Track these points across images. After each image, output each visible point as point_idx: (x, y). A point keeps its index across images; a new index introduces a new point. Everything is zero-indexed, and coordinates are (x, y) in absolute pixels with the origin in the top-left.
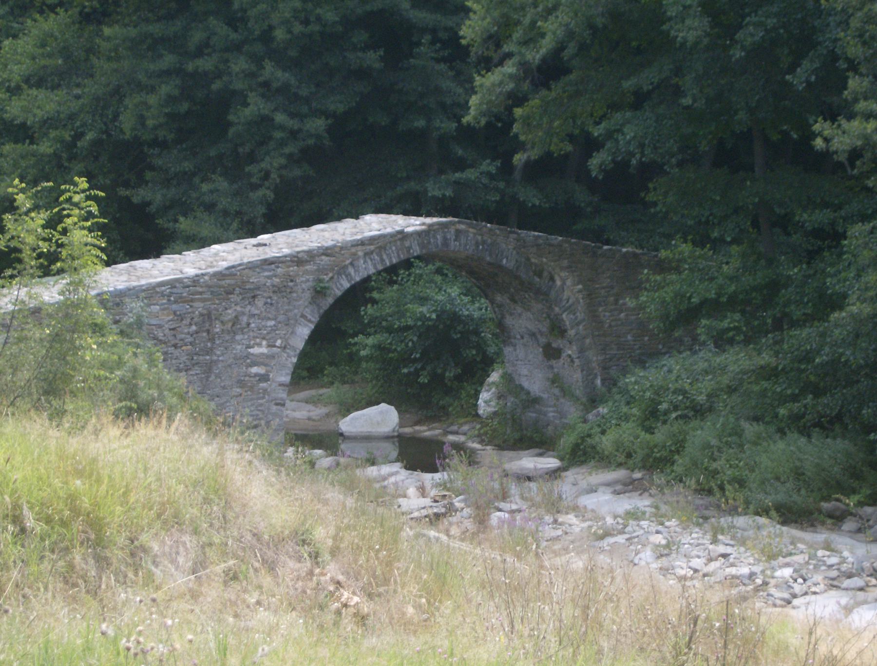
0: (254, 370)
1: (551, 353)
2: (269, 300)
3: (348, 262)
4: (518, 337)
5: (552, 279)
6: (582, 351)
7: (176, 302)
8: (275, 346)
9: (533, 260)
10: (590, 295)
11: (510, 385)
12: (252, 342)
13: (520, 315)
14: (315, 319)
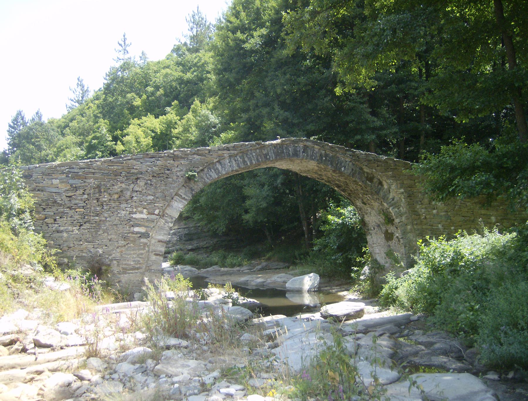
0: (136, 229)
1: (389, 236)
2: (149, 182)
3: (215, 161)
4: (372, 229)
5: (381, 183)
6: (404, 233)
7: (73, 178)
8: (154, 214)
9: (366, 170)
10: (410, 196)
12: (135, 210)
14: (189, 197)
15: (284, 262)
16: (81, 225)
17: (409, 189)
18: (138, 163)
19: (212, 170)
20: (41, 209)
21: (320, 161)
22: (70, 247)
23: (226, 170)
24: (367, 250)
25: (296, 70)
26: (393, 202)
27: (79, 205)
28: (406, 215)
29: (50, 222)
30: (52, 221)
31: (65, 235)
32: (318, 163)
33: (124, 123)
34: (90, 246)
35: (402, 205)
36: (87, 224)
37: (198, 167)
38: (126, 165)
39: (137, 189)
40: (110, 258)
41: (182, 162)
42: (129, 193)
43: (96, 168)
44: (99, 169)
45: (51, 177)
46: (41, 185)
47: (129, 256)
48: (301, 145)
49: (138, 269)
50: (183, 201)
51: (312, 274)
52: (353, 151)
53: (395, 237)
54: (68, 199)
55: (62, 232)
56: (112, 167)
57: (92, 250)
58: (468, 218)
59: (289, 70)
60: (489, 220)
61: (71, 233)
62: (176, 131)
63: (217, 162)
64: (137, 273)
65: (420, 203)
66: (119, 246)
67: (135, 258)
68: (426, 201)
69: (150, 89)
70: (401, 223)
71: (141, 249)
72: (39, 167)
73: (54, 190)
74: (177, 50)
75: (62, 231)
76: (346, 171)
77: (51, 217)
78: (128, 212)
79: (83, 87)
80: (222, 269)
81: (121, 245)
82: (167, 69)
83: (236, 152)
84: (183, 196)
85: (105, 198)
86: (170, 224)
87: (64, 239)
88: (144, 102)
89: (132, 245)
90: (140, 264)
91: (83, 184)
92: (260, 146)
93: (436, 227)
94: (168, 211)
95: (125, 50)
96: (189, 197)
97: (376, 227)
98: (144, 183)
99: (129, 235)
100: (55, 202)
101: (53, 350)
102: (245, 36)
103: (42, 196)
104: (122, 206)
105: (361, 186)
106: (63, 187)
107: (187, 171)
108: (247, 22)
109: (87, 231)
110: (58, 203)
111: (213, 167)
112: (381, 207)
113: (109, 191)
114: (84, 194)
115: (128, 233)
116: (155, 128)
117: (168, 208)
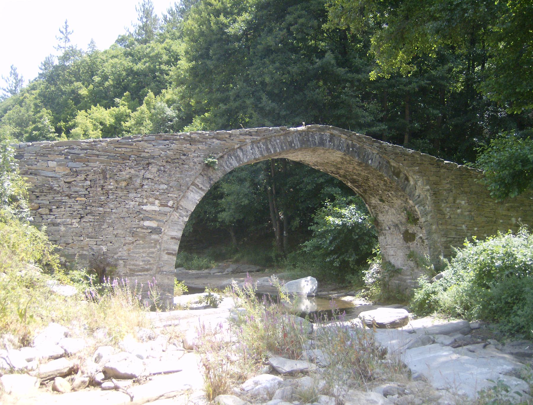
0: (147, 223)
1: (409, 237)
2: (162, 168)
3: (236, 146)
4: (387, 228)
5: (407, 179)
6: (429, 233)
7: (73, 160)
8: (167, 206)
9: (392, 164)
10: (435, 194)
11: (386, 265)
12: (145, 201)
13: (387, 212)
14: (207, 187)
15: (255, 264)
16: (81, 218)
17: (435, 186)
18: (149, 145)
19: (233, 157)
20: (33, 197)
21: (347, 152)
22: (68, 244)
23: (248, 157)
24: (378, 251)
25: (286, 58)
26: (419, 199)
27: (80, 193)
28: (431, 214)
29: (43, 213)
30: (47, 212)
31: (63, 228)
32: (344, 155)
33: (68, 114)
34: (92, 242)
35: (428, 203)
36: (89, 216)
37: (217, 154)
38: (136, 147)
39: (149, 176)
40: (116, 257)
41: (200, 146)
42: (139, 181)
43: (100, 150)
44: (105, 151)
45: (47, 158)
46: (34, 167)
47: (137, 256)
48: (328, 133)
49: (147, 270)
50: (200, 192)
51: (309, 278)
52: (380, 143)
53: (417, 238)
54: (67, 185)
55: (58, 225)
56: (120, 150)
57: (95, 247)
58: (491, 219)
59: (279, 57)
60: (510, 222)
61: (70, 226)
62: (128, 124)
63: (238, 148)
64: (146, 275)
65: (445, 201)
66: (127, 243)
67: (144, 257)
68: (451, 199)
69: (97, 79)
70: (426, 223)
71: (152, 247)
72: (33, 145)
73: (51, 174)
74: (121, 40)
75: (59, 224)
76: (373, 165)
77: (45, 206)
78: (137, 203)
79: (17, 76)
80: (190, 271)
81: (128, 242)
82: (116, 59)
83: (259, 138)
84: (201, 186)
85: (111, 185)
86: (185, 218)
87: (61, 233)
88: (91, 92)
89: (141, 242)
90: (150, 264)
91: (85, 168)
92: (284, 133)
93: (460, 228)
94: (183, 203)
95: (66, 37)
96: (207, 187)
97: (392, 227)
98: (156, 169)
99: (138, 230)
100: (52, 188)
101: (138, 381)
102: (228, 20)
103: (35, 180)
104: (131, 195)
105: (385, 181)
106: (61, 171)
107: (206, 157)
108: (229, 5)
109: (88, 224)
110: (55, 190)
111: (234, 154)
112: (404, 205)
113: (116, 177)
114: (86, 179)
115: (138, 228)
116: (105, 119)
117: (183, 200)
